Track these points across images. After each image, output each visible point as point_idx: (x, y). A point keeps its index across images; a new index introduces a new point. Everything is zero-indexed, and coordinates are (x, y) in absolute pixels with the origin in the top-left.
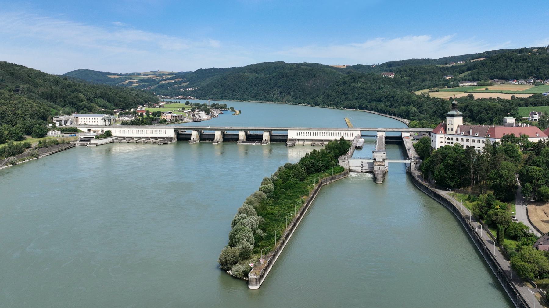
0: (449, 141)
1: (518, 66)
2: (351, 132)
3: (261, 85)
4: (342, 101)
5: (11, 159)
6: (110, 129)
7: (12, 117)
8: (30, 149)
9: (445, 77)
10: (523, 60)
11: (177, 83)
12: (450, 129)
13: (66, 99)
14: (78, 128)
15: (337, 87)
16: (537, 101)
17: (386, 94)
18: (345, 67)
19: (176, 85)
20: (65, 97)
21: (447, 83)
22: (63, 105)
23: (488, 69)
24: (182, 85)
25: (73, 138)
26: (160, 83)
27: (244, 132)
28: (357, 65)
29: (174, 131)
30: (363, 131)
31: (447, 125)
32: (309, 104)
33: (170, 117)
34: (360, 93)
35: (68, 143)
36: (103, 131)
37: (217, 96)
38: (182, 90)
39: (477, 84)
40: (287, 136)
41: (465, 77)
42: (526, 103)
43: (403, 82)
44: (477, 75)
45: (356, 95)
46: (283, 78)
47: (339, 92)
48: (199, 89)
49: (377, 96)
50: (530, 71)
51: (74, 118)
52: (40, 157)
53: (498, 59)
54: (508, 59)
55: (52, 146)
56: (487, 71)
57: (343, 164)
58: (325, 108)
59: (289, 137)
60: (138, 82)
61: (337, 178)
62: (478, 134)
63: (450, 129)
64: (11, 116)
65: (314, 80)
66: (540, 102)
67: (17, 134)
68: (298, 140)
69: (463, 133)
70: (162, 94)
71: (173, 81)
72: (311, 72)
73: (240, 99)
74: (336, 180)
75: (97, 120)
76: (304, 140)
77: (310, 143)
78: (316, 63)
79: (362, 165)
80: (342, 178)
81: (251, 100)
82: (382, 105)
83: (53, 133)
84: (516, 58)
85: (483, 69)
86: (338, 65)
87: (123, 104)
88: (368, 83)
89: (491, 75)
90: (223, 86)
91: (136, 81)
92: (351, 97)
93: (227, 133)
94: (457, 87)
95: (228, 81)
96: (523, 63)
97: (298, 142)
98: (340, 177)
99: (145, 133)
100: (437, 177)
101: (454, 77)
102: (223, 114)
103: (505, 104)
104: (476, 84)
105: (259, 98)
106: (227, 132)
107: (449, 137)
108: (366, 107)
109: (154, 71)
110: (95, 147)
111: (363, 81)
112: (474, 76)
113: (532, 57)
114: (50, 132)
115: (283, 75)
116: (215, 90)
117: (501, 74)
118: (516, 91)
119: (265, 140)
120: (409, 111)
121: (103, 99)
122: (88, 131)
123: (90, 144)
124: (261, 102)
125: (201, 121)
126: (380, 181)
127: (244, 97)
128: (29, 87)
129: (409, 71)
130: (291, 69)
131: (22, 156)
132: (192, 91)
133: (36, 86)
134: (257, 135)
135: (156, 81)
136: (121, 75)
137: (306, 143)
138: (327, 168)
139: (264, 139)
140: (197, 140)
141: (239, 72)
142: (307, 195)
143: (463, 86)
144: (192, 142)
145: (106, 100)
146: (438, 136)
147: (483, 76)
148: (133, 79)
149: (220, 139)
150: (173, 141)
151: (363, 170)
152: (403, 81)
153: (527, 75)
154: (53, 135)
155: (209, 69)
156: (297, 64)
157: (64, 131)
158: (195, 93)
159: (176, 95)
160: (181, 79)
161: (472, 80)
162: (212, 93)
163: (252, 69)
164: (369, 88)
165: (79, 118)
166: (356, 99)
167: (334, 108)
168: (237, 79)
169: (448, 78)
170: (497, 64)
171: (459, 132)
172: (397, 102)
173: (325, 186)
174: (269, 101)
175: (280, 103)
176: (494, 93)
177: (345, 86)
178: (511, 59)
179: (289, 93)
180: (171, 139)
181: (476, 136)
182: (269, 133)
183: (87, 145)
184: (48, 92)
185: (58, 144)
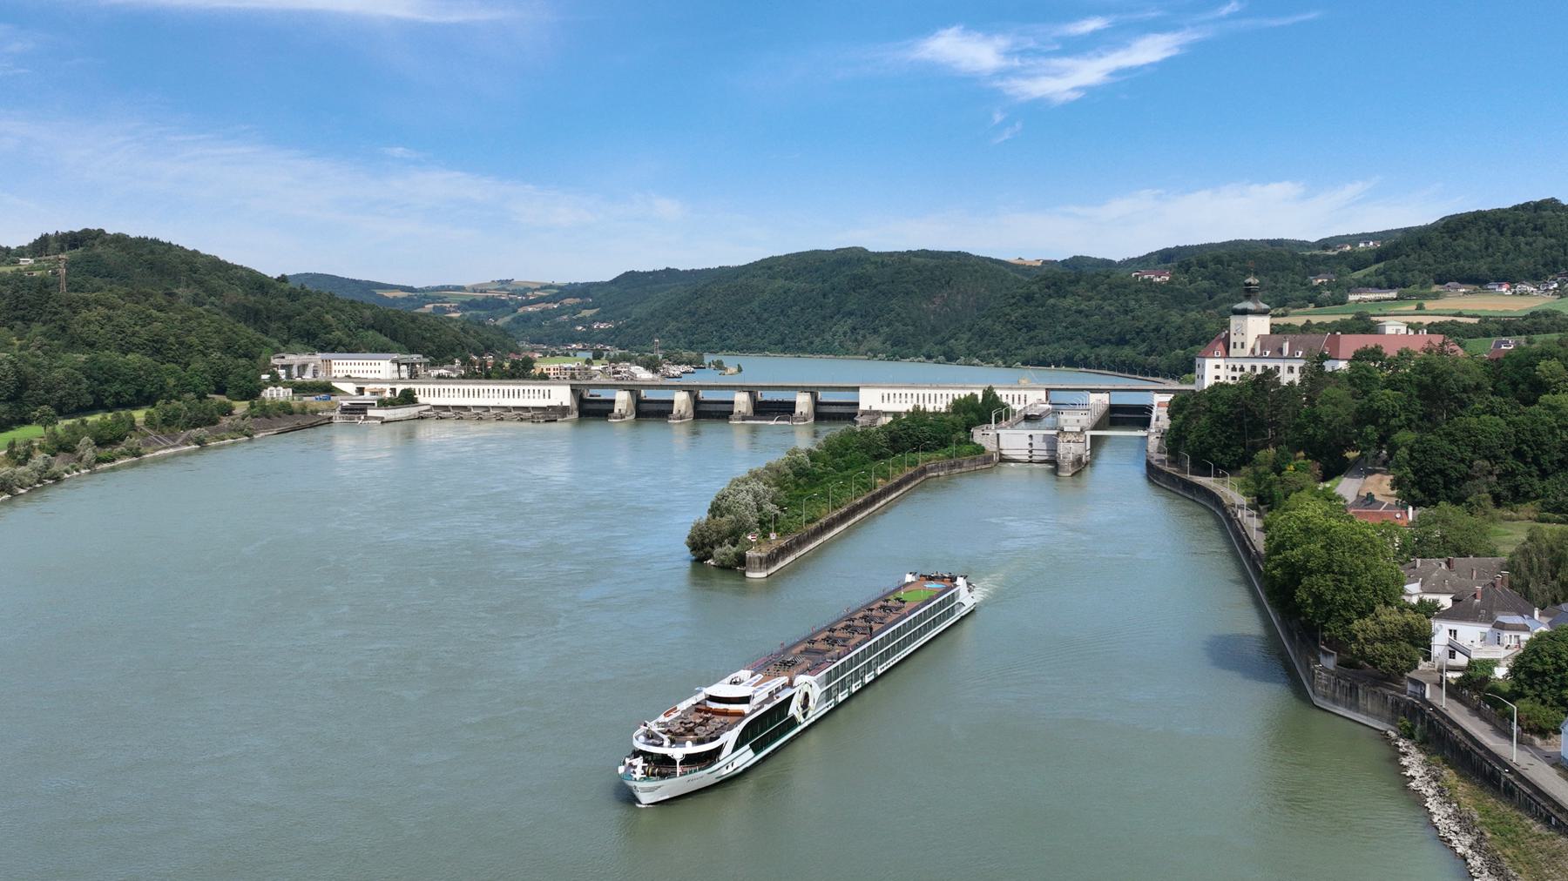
0: (1234, 374)
1: (1519, 245)
2: (1022, 393)
3: (799, 308)
4: (1021, 347)
5: (195, 432)
6: (412, 386)
8: (232, 417)
9: (1311, 278)
11: (567, 310)
12: (1239, 345)
13: (291, 324)
14: (333, 384)
15: (1007, 310)
16: (1535, 323)
17: (1141, 324)
18: (1039, 264)
19: (565, 317)
20: (289, 318)
21: (1314, 294)
22: (285, 337)
23: (1435, 256)
24: (579, 315)
25: (323, 405)
26: (521, 310)
27: (747, 393)
28: (1074, 257)
29: (572, 390)
30: (1052, 390)
32: (929, 357)
33: (556, 372)
34: (1071, 324)
36: (393, 391)
37: (678, 342)
38: (581, 328)
39: (1399, 295)
40: (858, 404)
41: (1368, 278)
43: (1192, 294)
44: (1401, 272)
46: (861, 290)
47: (1012, 322)
48: (626, 323)
49: (1116, 331)
50: (1551, 259)
51: (320, 362)
52: (255, 436)
53: (1464, 227)
54: (1494, 227)
55: (279, 416)
56: (1431, 261)
57: (984, 439)
58: (973, 365)
59: (863, 407)
61: (965, 465)
62: (1300, 353)
63: (1239, 345)
64: (174, 348)
65: (946, 295)
66: (1543, 326)
67: (196, 386)
69: (1268, 353)
70: (526, 340)
71: (556, 307)
72: (938, 273)
74: (963, 470)
75: (377, 368)
78: (954, 252)
79: (1031, 444)
80: (977, 468)
81: (769, 351)
82: (1126, 352)
83: (275, 393)
84: (1515, 223)
85: (1419, 256)
86: (1020, 258)
88: (1096, 297)
89: (1439, 272)
90: (694, 314)
91: (454, 307)
92: (1045, 335)
93: (706, 399)
94: (1341, 304)
95: (709, 301)
96: (1533, 236)
97: (884, 418)
98: (973, 464)
99: (499, 397)
100: (1193, 445)
102: (693, 372)
104: (1393, 294)
105: (793, 344)
106: (704, 395)
107: (1234, 363)
108: (1083, 359)
109: (501, 282)
110: (378, 425)
112: (1391, 275)
113: (1562, 221)
114: (268, 391)
115: (859, 283)
117: (1467, 267)
118: (1502, 312)
119: (802, 413)
121: (381, 332)
122: (356, 392)
123: (367, 418)
124: (799, 357)
126: (1068, 471)
127: (752, 344)
128: (197, 295)
129: (1212, 266)
130: (883, 265)
131: (217, 431)
133: (211, 292)
134: (780, 402)
135: (507, 306)
136: (411, 289)
138: (943, 444)
139: (798, 410)
140: (628, 413)
141: (737, 277)
142: (887, 479)
143: (1359, 301)
144: (616, 418)
145: (386, 335)
146: (1210, 363)
147: (1416, 272)
148: (446, 300)
149: (686, 412)
150: (569, 417)
151: (1034, 458)
152: (1194, 292)
153: (1542, 270)
154: (276, 394)
155: (654, 273)
156: (902, 254)
157: (300, 389)
158: (617, 336)
159: (564, 341)
160: (578, 300)
161: (1385, 285)
162: (664, 333)
163: (768, 266)
164: (1097, 311)
165: (333, 362)
166: (1058, 340)
167: (997, 366)
168: (733, 295)
169: (1320, 281)
170: (1460, 241)
171: (1258, 352)
172: (1167, 340)
173: (935, 479)
175: (851, 357)
177: (1031, 306)
178: (1501, 226)
179: (875, 331)
180: (563, 411)
181: (1296, 356)
182: (812, 397)
183: (360, 422)
184: (247, 304)
185: (291, 413)
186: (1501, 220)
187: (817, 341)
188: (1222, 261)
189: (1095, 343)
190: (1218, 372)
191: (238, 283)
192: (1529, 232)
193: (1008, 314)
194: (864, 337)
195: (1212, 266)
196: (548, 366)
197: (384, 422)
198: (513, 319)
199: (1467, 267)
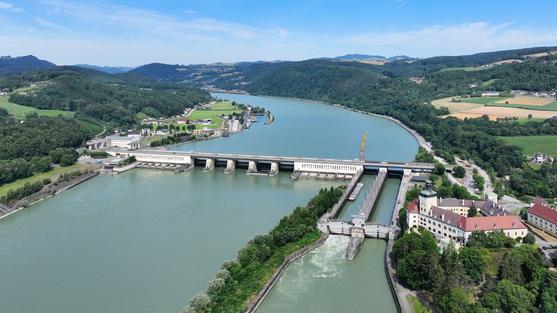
2: (354, 166)
4: (371, 106)
6: (135, 154)
7: (46, 145)
10: (546, 71)
12: (423, 210)
13: (111, 114)
26: (221, 76)
29: (191, 158)
31: (420, 205)
35: (92, 172)
36: (129, 155)
39: (499, 95)
41: (489, 87)
42: (538, 131)
45: (384, 100)
49: (402, 105)
53: (522, 69)
56: (510, 81)
59: (296, 168)
60: (201, 75)
62: (449, 221)
63: (423, 210)
64: (44, 145)
67: (43, 166)
68: (304, 172)
73: (284, 96)
76: (309, 172)
77: (315, 174)
87: (169, 112)
89: (513, 86)
92: (379, 102)
94: (480, 97)
101: (478, 85)
103: (516, 132)
104: (498, 94)
107: (422, 217)
109: (218, 63)
111: (392, 86)
114: (81, 158)
116: (264, 86)
117: (523, 85)
120: (425, 130)
121: (152, 107)
125: (230, 135)
126: (352, 258)
129: (436, 77)
132: (245, 86)
137: (312, 174)
143: (486, 96)
148: (198, 72)
149: (231, 168)
151: (344, 233)
152: (430, 87)
159: (231, 89)
160: (238, 73)
162: (261, 89)
165: (112, 140)
170: (521, 74)
171: (431, 215)
174: (303, 98)
176: (514, 107)
179: (326, 93)
180: (188, 165)
186: (534, 67)
187: (308, 95)
188: (440, 76)
189: (396, 109)
190: (415, 219)
191: (104, 92)
192: (545, 72)
193: (368, 93)
194: (323, 95)
195: (436, 77)
196: (198, 130)
197: (119, 173)
198: (218, 79)
199: (523, 85)
